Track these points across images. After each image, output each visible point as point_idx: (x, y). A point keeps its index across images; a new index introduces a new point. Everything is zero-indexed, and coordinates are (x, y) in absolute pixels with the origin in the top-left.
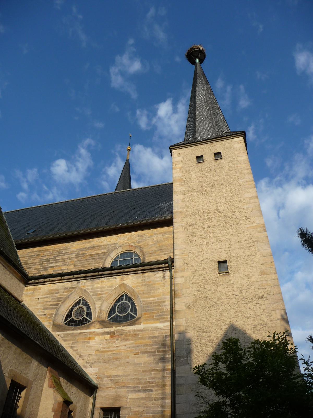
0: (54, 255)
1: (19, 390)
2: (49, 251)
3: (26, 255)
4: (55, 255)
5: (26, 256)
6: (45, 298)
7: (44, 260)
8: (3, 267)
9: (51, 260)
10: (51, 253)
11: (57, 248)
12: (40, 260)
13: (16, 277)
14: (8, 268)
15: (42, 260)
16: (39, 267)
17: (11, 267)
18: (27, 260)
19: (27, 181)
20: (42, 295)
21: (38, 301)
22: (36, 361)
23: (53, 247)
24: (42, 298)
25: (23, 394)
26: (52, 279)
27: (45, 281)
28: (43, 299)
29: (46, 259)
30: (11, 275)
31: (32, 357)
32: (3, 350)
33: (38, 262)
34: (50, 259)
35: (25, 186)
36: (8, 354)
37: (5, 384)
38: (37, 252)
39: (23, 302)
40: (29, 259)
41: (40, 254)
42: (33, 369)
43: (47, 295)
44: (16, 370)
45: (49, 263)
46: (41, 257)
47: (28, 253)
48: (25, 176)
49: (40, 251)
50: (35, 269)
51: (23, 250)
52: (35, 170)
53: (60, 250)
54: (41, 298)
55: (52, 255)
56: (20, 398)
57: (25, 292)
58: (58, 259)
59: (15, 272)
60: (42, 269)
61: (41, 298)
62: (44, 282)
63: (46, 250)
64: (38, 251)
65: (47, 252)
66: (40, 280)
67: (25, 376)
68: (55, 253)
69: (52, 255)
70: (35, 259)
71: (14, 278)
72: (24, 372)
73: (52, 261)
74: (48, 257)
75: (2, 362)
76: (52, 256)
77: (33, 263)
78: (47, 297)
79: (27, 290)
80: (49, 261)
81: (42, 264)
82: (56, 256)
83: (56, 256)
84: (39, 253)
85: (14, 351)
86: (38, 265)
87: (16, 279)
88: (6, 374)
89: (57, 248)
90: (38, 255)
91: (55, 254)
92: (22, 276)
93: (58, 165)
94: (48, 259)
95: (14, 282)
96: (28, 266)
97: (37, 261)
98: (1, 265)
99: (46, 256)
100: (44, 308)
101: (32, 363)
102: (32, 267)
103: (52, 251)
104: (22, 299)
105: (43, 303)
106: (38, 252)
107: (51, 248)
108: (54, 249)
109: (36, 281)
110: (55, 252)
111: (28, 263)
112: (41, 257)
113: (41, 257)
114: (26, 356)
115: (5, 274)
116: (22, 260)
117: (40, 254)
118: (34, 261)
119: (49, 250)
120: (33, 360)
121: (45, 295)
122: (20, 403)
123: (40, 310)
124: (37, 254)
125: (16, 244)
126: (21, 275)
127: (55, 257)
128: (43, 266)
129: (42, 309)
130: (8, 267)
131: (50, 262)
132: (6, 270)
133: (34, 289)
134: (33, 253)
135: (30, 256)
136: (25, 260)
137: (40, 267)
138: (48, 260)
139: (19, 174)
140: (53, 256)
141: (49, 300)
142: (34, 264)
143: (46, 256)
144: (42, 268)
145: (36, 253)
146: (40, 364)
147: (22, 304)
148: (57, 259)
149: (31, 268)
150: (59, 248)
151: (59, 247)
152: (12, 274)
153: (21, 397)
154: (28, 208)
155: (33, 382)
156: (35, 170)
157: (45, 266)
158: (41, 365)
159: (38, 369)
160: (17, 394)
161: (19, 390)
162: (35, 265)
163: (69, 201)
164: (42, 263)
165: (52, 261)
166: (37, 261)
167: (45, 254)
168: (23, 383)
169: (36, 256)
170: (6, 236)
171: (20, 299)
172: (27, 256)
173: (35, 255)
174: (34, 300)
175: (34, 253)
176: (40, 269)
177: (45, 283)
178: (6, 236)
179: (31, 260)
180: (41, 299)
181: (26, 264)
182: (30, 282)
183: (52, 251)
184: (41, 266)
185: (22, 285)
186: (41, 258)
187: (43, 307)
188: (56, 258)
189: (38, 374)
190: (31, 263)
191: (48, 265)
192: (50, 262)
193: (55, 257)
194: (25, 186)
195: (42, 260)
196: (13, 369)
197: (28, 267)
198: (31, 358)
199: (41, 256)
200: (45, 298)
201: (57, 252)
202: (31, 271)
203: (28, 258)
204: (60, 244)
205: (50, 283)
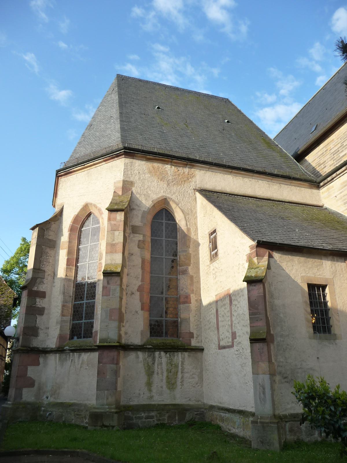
0: (340, 142)
1: (321, 288)
2: (334, 142)
3: (316, 157)
4: (342, 142)
5: (316, 157)
6: (341, 193)
7: (333, 152)
8: (286, 186)
9: (339, 149)
10: (337, 142)
11: (339, 135)
12: (330, 155)
13: (304, 188)
14: (292, 184)
15: (332, 154)
16: (333, 162)
17: (294, 181)
18: (319, 161)
19: (317, 62)
20: (338, 192)
21: (337, 199)
22: (328, 261)
23: (336, 135)
24: (339, 194)
25: (327, 290)
26: (338, 172)
27: (333, 177)
28: (339, 195)
29: (335, 151)
30: (298, 188)
31: (321, 259)
32: (285, 264)
33: (330, 158)
34: (338, 149)
35: (318, 68)
36: (292, 265)
37: (302, 289)
38: (324, 149)
39: (324, 206)
40: (320, 159)
41: (327, 149)
42: (327, 268)
43: (341, 189)
44: (308, 275)
45: (340, 153)
46: (330, 151)
47: (317, 153)
48: (311, 59)
49: (326, 146)
50: (330, 166)
51: (311, 153)
52: (317, 45)
53: (344, 134)
54: (337, 195)
55: (339, 143)
56: (326, 295)
57: (322, 196)
58: (345, 144)
59: (301, 184)
60: (323, 166)
61: (337, 195)
62: (333, 179)
63: (331, 142)
64: (324, 147)
65: (333, 143)
66: (329, 179)
67: (322, 277)
68: (340, 139)
69: (339, 143)
70: (325, 156)
71: (303, 189)
72: (318, 274)
73: (341, 149)
74: (336, 148)
75: (290, 273)
76: (339, 144)
77: (325, 161)
78: (343, 192)
79: (323, 193)
80: (339, 151)
81: (334, 157)
82: (343, 142)
83: (343, 142)
84: (326, 148)
85: (297, 261)
86: (330, 160)
87: (305, 189)
88: (299, 281)
89: (339, 135)
90: (326, 151)
91: (341, 140)
92: (309, 183)
93: (338, 20)
94: (336, 150)
95: (305, 193)
96: (322, 166)
97: (328, 156)
98: (283, 185)
99: (333, 148)
100: (345, 202)
101: (324, 264)
102: (326, 165)
103: (337, 139)
104: (323, 203)
105: (341, 198)
106: (325, 148)
107: (334, 138)
108: (337, 137)
109: (326, 181)
110: (339, 139)
111: (321, 163)
112: (329, 151)
113: (329, 151)
114: (314, 261)
115: (291, 190)
116: (314, 165)
117: (327, 148)
118: (326, 159)
119: (333, 140)
120: (324, 261)
121: (340, 190)
122: (328, 298)
123: (341, 206)
124: (325, 150)
125: (292, 156)
126: (307, 183)
127: (343, 144)
128: (336, 159)
129: (343, 204)
130: (291, 183)
131: (340, 151)
132: (290, 186)
133: (328, 189)
134: (321, 151)
135: (320, 156)
136: (317, 162)
137: (333, 161)
138: (337, 150)
139: (303, 61)
140: (340, 144)
141: (345, 193)
142: (327, 161)
143: (333, 148)
144: (336, 162)
145: (323, 150)
146: (334, 262)
147: (324, 207)
148: (345, 145)
149: (325, 167)
150: (341, 133)
151: (341, 132)
152: (299, 186)
153: (327, 294)
154: (307, 104)
155: (333, 278)
156: (317, 45)
157: (337, 158)
158: (336, 262)
159: (334, 267)
160: (321, 292)
161: (321, 288)
162: (328, 162)
163: (341, 68)
164: (333, 157)
165: (341, 149)
166: (328, 156)
167: (331, 146)
168: (324, 283)
169: (324, 153)
170: (280, 155)
171: (320, 204)
172: (317, 157)
173: (323, 153)
174: (333, 199)
175: (322, 151)
176: (334, 163)
177: (335, 179)
178: (280, 155)
179: (322, 159)
180: (338, 196)
181: (320, 165)
182: (322, 184)
183: (337, 139)
184: (333, 161)
185: (315, 191)
186: (330, 152)
187: (343, 203)
188: (343, 144)
189: (336, 271)
190: (323, 163)
191: (339, 156)
192: (340, 151)
193: (343, 144)
194: (318, 68)
195: (332, 154)
196: (304, 275)
197: (323, 167)
198: (320, 260)
199: (329, 150)
200: (341, 193)
201: (342, 137)
202: (327, 169)
203: (319, 158)
204: (341, 128)
205: (338, 177)
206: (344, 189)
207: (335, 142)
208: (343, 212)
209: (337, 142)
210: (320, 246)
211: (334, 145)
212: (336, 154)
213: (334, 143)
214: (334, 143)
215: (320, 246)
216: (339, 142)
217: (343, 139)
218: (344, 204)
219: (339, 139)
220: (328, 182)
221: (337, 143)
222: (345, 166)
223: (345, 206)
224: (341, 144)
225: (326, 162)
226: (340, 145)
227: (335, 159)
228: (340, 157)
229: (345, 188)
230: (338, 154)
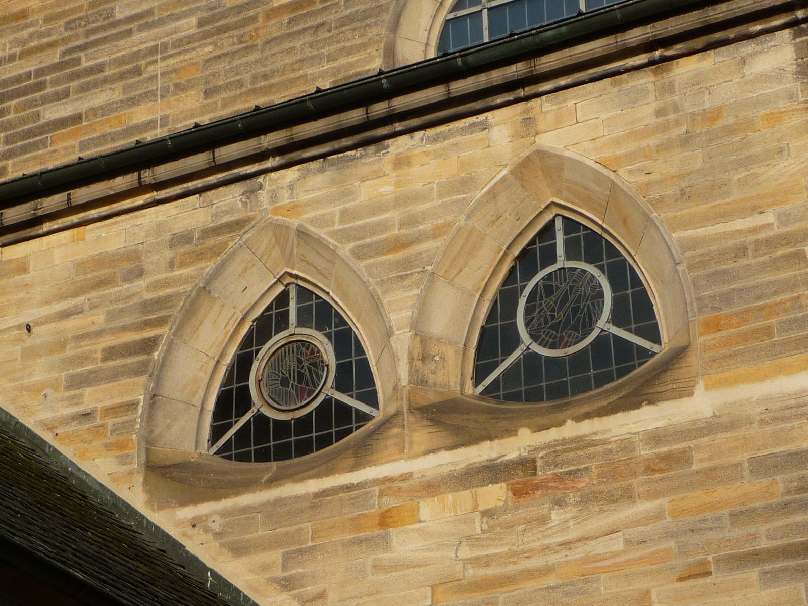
0: (64, 41)
2: (26, 26)
6: (65, 315)
9: (48, 78)
10: (42, 35)
21: (29, 341)
26: (81, 194)
27: (40, 213)
28: (52, 326)
29: (18, 79)
34: (40, 72)
43: (75, 295)
45: (45, 100)
54: (38, 323)
58: (91, 63)
60: (17, 110)
61: (38, 323)
62: (37, 221)
68: (68, 26)
73: (56, 82)
74: (30, 65)
76: (50, 51)
78: (77, 311)
80: (40, 86)
94: (28, 75)
103: (47, 20)
105: (61, 345)
110: (62, 22)
121: (61, 297)
123: (49, 391)
127: (75, 55)
131: (49, 90)
157: (23, 121)
177: (47, 227)
183: (47, 20)
192: (49, 90)
193: (75, 55)
200: (65, 315)
201: (80, 18)
205: (75, 218)
206: (88, 296)
207: (32, 30)
208: (50, 429)
209: (42, 35)
210: (83, 557)
211: (25, 43)
212: (19, 96)
213: (25, 33)
214: (25, 33)
215: (83, 557)
216: (54, 38)
217: (80, 31)
218: (68, 387)
219: (62, 22)
220: (628, 70)
221: (45, 40)
222: (136, 174)
223: (74, 397)
224: (64, 54)
225: (100, 76)
226: (55, 56)
227: (9, 121)
228: (42, 121)
229: (94, 294)
230: (33, 104)
